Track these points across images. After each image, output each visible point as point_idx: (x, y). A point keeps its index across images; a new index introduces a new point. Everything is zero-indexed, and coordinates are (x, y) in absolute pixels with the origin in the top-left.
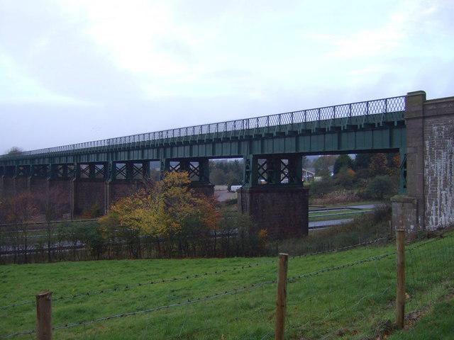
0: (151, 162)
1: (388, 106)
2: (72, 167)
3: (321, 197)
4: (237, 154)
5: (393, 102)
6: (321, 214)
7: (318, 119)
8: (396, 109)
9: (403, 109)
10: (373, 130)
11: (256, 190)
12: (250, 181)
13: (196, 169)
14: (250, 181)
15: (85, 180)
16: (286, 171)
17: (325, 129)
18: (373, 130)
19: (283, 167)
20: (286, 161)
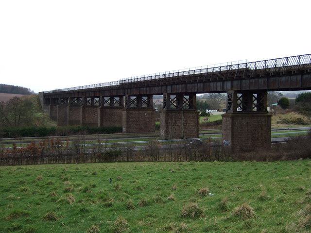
0: (153, 96)
1: (300, 61)
2: (82, 99)
3: (205, 190)
4: (202, 91)
5: (306, 57)
6: (293, 100)
7: (255, 69)
8: (306, 63)
9: (273, 140)
10: (276, 67)
11: (236, 115)
12: (232, 109)
13: (187, 100)
14: (232, 109)
15: (107, 107)
16: (255, 102)
17: (259, 75)
18: (276, 67)
19: (254, 98)
20: (256, 95)
